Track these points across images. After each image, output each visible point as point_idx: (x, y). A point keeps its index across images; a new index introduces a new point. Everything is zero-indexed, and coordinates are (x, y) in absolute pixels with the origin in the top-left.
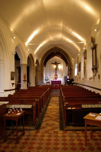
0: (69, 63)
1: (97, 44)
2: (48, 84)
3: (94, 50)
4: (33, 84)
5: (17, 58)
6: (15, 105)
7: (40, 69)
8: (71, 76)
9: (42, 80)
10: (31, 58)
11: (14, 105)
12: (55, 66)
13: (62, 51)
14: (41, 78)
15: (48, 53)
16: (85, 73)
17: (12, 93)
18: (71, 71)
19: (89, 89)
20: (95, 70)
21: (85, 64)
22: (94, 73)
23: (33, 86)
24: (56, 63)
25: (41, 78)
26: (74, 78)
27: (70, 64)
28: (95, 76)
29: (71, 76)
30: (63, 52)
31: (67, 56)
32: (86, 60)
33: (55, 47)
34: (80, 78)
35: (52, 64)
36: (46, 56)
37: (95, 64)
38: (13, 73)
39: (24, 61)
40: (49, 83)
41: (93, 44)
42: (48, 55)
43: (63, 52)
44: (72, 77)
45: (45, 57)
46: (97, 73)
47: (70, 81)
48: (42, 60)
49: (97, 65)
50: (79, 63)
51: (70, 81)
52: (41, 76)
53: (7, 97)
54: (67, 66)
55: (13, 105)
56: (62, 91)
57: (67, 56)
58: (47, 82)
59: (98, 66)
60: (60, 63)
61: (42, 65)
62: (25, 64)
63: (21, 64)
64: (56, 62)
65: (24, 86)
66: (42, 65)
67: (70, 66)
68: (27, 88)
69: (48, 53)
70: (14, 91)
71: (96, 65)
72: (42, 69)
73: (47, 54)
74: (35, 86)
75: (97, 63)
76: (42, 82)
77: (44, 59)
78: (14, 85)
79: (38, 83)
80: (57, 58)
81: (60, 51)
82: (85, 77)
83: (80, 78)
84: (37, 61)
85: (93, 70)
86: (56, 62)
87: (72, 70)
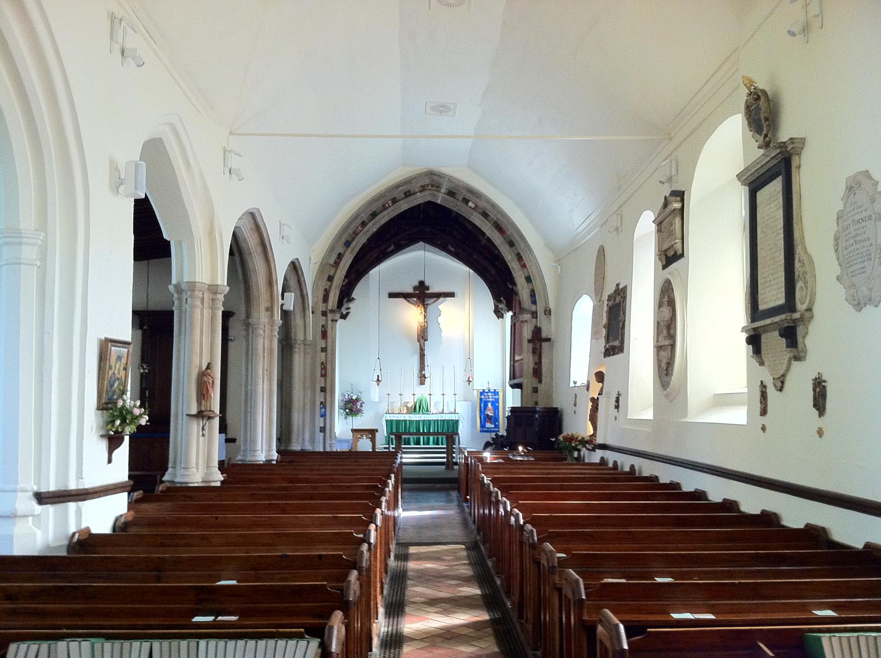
0: (523, 290)
1: (803, 141)
2: (365, 445)
3: (777, 185)
4: (264, 450)
5: (151, 242)
6: (156, 644)
7: (306, 329)
8: (535, 390)
9: (323, 416)
10: (251, 242)
11: (146, 645)
12: (412, 315)
13: (476, 208)
14: (320, 398)
15: (374, 215)
16: (670, 364)
17: (103, 516)
18: (534, 350)
19: (718, 490)
20: (773, 341)
21: (671, 303)
22: (762, 363)
23: (261, 457)
24: (422, 295)
25: (320, 398)
26: (561, 401)
27: (534, 302)
28: (763, 386)
29: (541, 387)
30: (485, 215)
31: (511, 244)
32: (674, 266)
33: (431, 174)
34: (617, 407)
35: (392, 295)
36: (355, 234)
37: (773, 295)
38: (115, 350)
39: (200, 264)
40: (372, 433)
41: (766, 145)
42: (373, 227)
43: (485, 215)
44: (549, 396)
45: (347, 244)
46: (795, 365)
47: (536, 427)
48: (332, 261)
49: (801, 307)
50: (610, 289)
51: (536, 427)
52: (320, 382)
53: (64, 553)
54: (499, 313)
55: (136, 644)
56: (383, 493)
57: (511, 244)
58: (354, 431)
59: (809, 310)
60: (451, 295)
61: (326, 299)
62: (213, 289)
63: (174, 281)
64: (422, 283)
65: (197, 459)
66: (326, 299)
67: (534, 315)
68: (217, 478)
69: (374, 215)
70: (117, 506)
71: (790, 305)
72: (324, 335)
73: (364, 224)
74: (275, 456)
75: (799, 285)
76: (323, 430)
77: (340, 256)
78: (123, 452)
79: (294, 436)
80: (420, 261)
81: (466, 201)
82: (228, 441)
83: (617, 407)
84: (294, 267)
85: (754, 340)
86: (422, 283)
87: (545, 345)
